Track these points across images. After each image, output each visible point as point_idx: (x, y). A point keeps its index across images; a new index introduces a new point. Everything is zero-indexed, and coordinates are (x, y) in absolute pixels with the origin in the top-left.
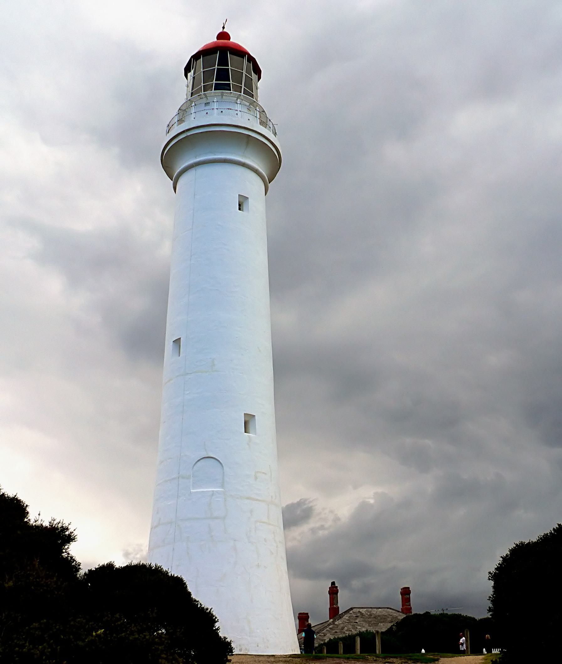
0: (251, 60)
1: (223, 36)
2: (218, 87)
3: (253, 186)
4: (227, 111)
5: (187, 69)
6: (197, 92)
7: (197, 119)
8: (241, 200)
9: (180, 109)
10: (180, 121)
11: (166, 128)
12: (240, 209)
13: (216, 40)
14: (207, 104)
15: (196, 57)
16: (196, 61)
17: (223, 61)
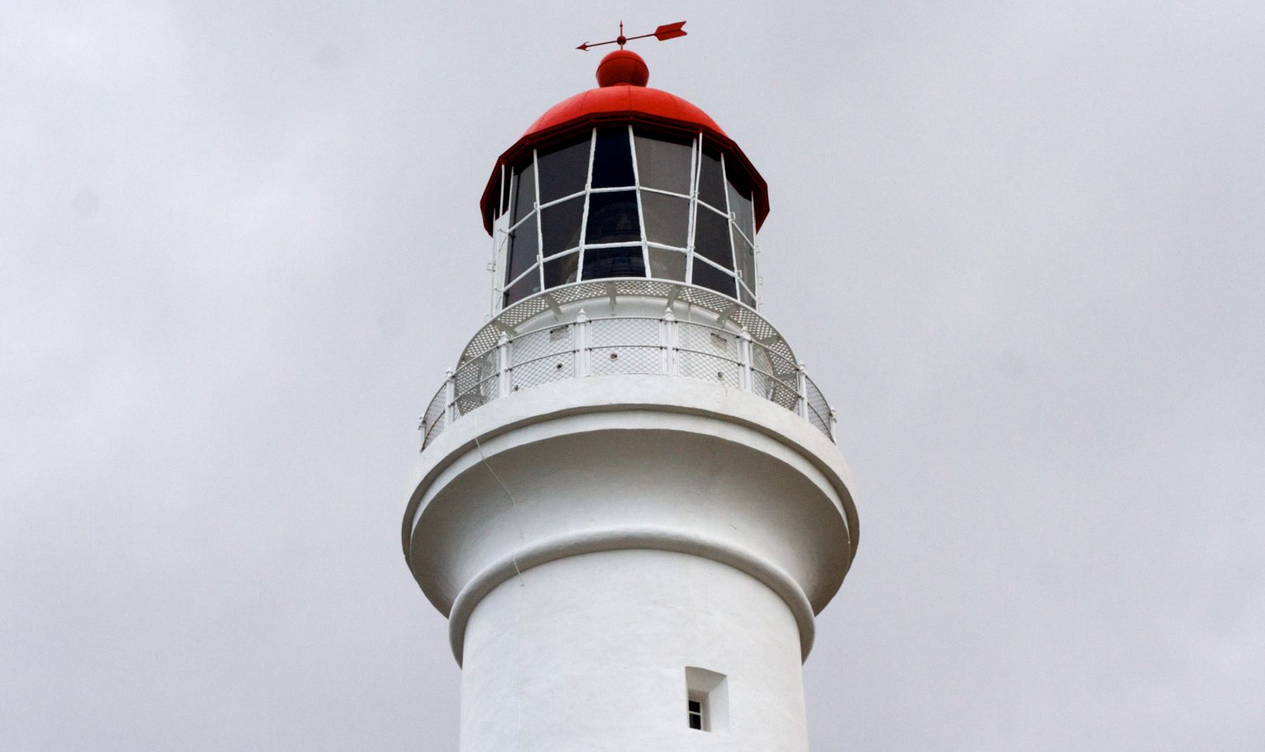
0: (721, 148)
1: (623, 69)
2: (598, 265)
3: (737, 624)
4: (636, 355)
5: (490, 207)
6: (528, 286)
7: (534, 392)
8: (700, 687)
9: (463, 358)
10: (468, 399)
11: (419, 436)
12: (695, 723)
13: (593, 84)
14: (558, 331)
15: (514, 160)
16: (518, 173)
17: (614, 167)
